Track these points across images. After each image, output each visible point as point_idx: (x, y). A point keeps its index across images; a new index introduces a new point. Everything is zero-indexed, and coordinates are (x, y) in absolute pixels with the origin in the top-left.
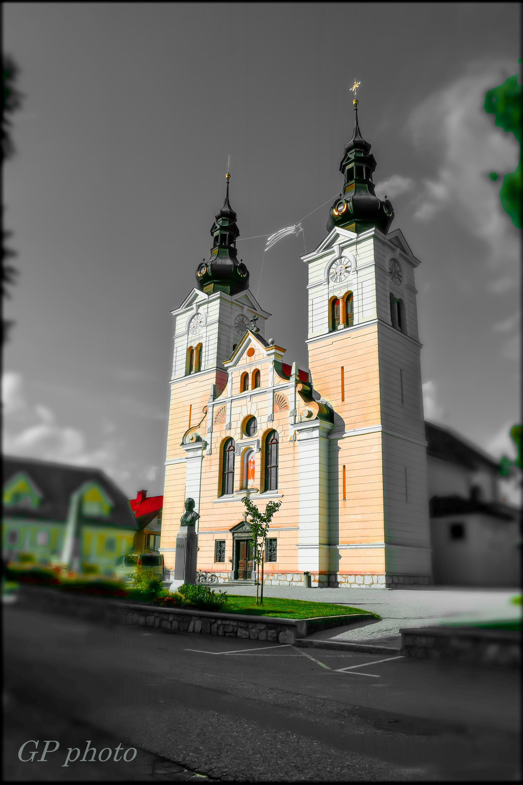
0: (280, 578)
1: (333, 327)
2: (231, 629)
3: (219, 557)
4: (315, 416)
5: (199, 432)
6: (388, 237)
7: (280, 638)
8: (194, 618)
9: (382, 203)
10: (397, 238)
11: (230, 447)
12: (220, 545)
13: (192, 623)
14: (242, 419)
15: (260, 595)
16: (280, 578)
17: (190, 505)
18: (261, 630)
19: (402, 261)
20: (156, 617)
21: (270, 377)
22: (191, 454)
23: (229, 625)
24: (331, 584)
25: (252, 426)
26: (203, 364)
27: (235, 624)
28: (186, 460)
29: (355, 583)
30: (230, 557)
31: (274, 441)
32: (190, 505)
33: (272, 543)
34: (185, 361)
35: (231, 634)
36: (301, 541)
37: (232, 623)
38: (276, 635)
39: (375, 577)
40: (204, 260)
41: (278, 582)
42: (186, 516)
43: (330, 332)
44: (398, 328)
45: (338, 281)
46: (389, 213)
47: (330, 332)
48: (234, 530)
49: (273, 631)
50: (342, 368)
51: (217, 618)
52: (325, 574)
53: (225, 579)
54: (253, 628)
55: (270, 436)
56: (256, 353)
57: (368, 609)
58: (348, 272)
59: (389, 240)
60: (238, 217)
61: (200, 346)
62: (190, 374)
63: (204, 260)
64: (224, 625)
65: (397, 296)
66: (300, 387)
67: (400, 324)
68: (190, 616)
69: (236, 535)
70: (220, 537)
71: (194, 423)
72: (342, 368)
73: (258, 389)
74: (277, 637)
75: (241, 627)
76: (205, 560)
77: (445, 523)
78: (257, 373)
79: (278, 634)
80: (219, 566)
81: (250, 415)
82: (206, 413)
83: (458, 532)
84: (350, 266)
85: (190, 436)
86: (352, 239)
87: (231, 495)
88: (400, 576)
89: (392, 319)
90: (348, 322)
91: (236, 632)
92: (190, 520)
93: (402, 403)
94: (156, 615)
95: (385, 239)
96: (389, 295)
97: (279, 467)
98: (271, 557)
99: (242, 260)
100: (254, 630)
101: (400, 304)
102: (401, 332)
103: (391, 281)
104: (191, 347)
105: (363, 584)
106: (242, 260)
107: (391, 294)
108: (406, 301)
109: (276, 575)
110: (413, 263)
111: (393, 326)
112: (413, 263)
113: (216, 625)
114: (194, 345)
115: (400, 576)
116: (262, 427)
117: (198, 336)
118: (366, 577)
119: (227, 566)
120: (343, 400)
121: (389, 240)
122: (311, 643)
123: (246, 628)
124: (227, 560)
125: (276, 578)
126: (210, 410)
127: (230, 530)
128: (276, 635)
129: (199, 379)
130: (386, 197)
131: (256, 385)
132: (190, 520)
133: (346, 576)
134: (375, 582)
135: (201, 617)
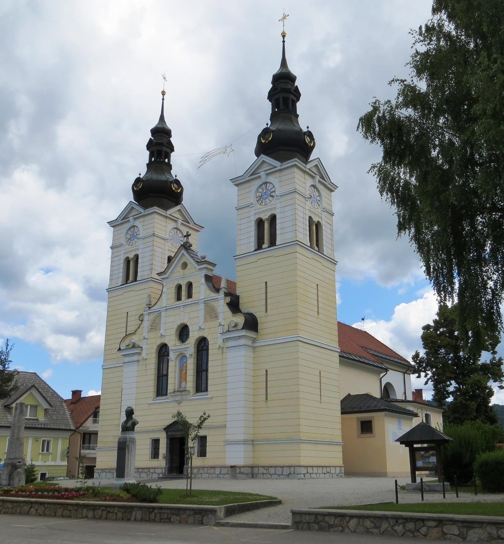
0: (209, 471)
1: (259, 246)
2: (166, 516)
3: (155, 454)
4: (241, 326)
5: (135, 339)
6: (309, 166)
7: (204, 521)
8: (135, 509)
9: (305, 133)
10: (316, 166)
11: (164, 352)
12: (156, 443)
13: (134, 513)
14: (176, 327)
15: (189, 488)
16: (209, 471)
17: (130, 413)
18: (189, 516)
19: (320, 187)
20: (103, 510)
21: (201, 290)
22: (127, 359)
23: (164, 513)
24: (255, 476)
25: (185, 333)
26: (139, 274)
27: (169, 511)
28: (122, 365)
29: (275, 474)
30: (164, 454)
31: (205, 348)
32: (130, 413)
33: (203, 440)
34: (121, 270)
35: (166, 520)
36: (229, 438)
37: (166, 511)
38: (201, 519)
39: (292, 469)
40: (140, 174)
41: (207, 475)
42: (126, 422)
43: (255, 250)
44: (316, 248)
45: (264, 204)
46: (310, 142)
47: (255, 250)
48: (167, 429)
49: (199, 516)
50: (266, 283)
51: (154, 508)
52: (249, 467)
53: (159, 474)
54: (183, 515)
55: (202, 345)
56: (189, 266)
57: (280, 497)
58: (273, 196)
59: (309, 169)
60: (173, 133)
61: (137, 257)
62: (127, 283)
63: (140, 174)
64: (160, 513)
65: (315, 219)
66: (228, 299)
67: (317, 245)
68: (132, 507)
69: (169, 433)
70: (155, 436)
71: (131, 330)
72: (266, 283)
73: (190, 300)
74: (202, 520)
75: (174, 514)
76: (141, 456)
77: (354, 419)
78: (190, 285)
79: (202, 518)
80: (155, 463)
81: (183, 324)
82: (142, 321)
83: (366, 427)
84: (274, 191)
85: (127, 342)
86: (276, 167)
87: (165, 397)
88: (315, 467)
89: (311, 240)
90: (273, 242)
91: (170, 519)
92: (130, 425)
93: (318, 314)
94: (103, 508)
95: (305, 168)
96: (308, 219)
97: (209, 371)
98: (203, 453)
99: (176, 176)
100: (184, 516)
101: (318, 225)
102: (318, 251)
103: (310, 205)
104: (128, 258)
105: (282, 474)
106: (176, 176)
107: (310, 218)
108: (323, 223)
109: (206, 469)
110: (331, 188)
111: (311, 247)
112: (331, 188)
113: (153, 514)
114: (131, 256)
115: (315, 467)
116: (194, 336)
117: (134, 248)
118: (285, 468)
119: (161, 463)
120: (266, 312)
121: (309, 169)
122: (228, 523)
123: (178, 515)
124: (161, 456)
125: (206, 472)
126: (146, 318)
127: (165, 429)
128: (201, 519)
129: (136, 288)
130: (308, 127)
131: (190, 295)
132: (130, 425)
133: (267, 468)
134: (292, 472)
135: (141, 508)
